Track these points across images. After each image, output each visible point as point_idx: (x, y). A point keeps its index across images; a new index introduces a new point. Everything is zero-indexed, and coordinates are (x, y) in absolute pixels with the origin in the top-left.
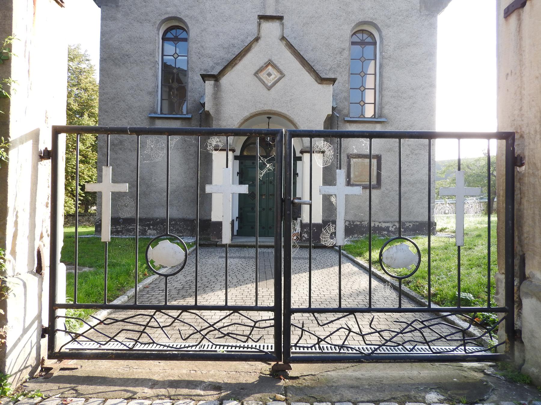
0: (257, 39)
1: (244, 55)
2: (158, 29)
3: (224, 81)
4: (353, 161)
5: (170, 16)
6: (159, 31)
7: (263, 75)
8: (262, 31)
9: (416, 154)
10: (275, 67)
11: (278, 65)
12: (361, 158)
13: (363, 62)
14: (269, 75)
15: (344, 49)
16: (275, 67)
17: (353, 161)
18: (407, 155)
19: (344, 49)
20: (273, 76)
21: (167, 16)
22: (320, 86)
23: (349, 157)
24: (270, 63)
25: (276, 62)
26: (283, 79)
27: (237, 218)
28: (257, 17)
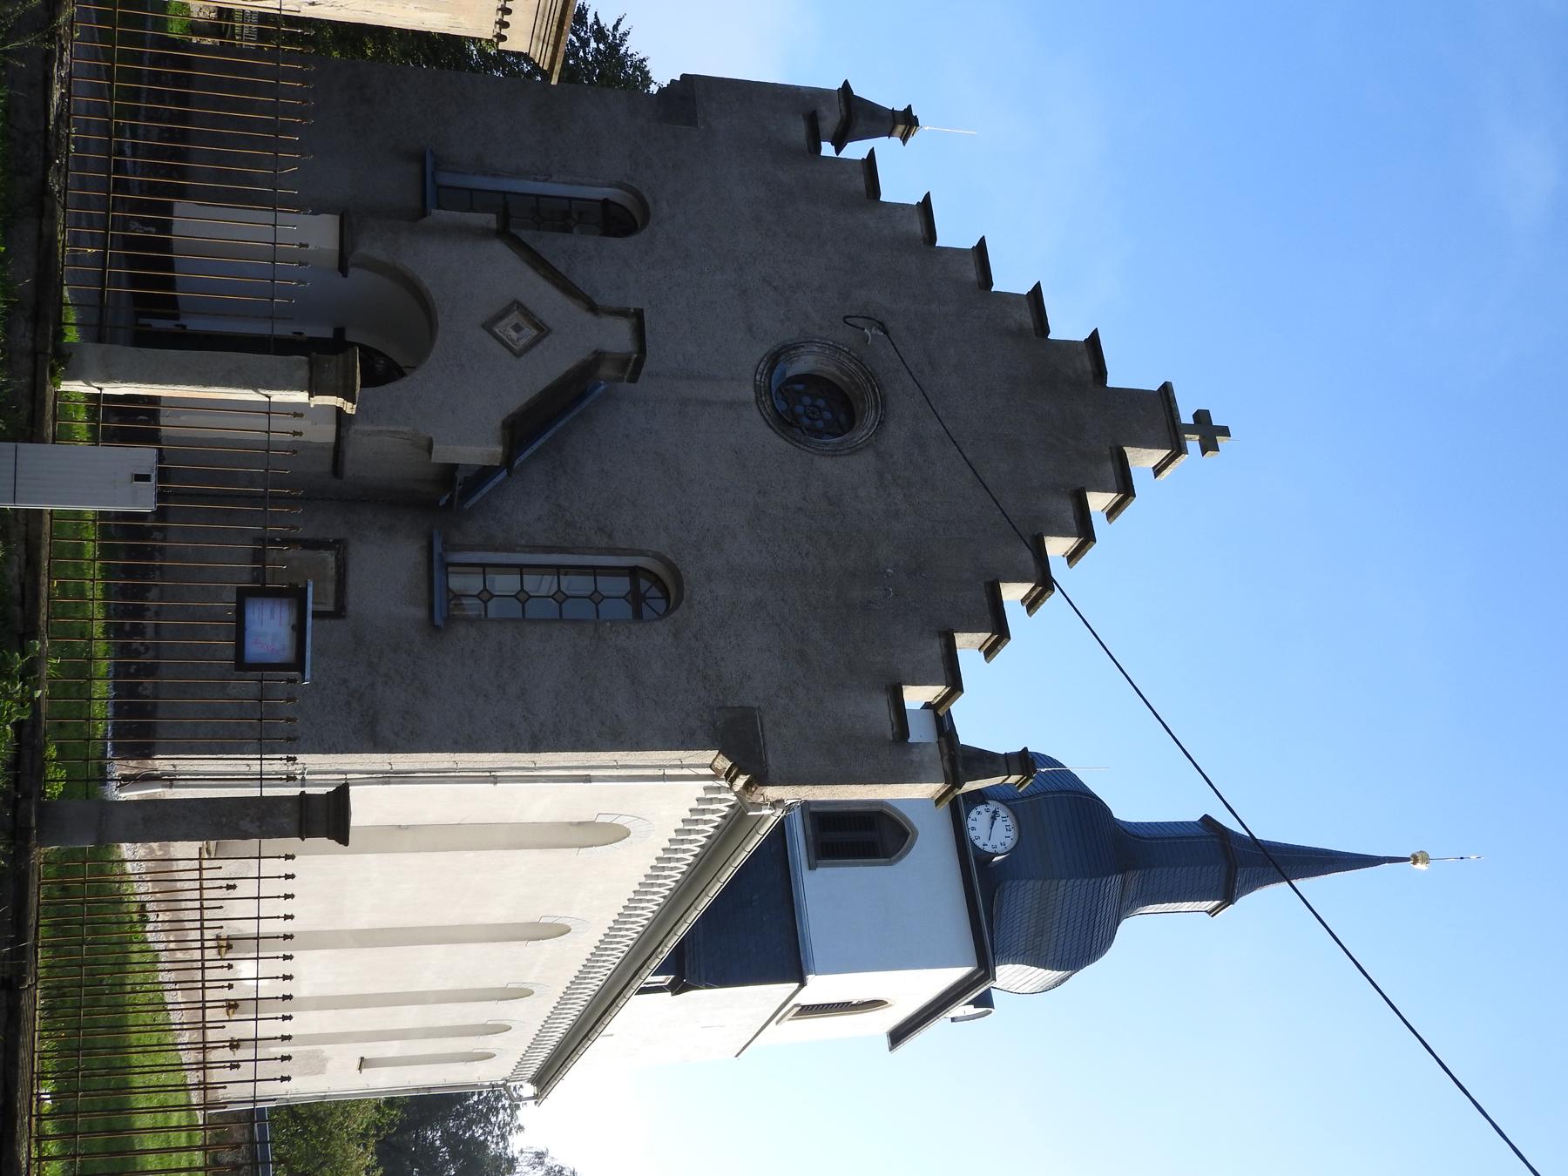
0: (593, 308)
1: (557, 285)
2: (619, 185)
3: (499, 248)
4: (329, 557)
5: (651, 206)
6: (610, 186)
7: (515, 317)
8: (611, 319)
9: (348, 703)
10: (535, 342)
11: (540, 346)
12: (338, 572)
13: (589, 597)
14: (517, 328)
15: (610, 536)
16: (535, 342)
17: (329, 557)
18: (345, 681)
19: (610, 536)
20: (514, 335)
21: (649, 200)
22: (499, 424)
23: (338, 546)
24: (543, 330)
25: (545, 341)
26: (508, 353)
27: (184, 327)
28: (639, 306)
